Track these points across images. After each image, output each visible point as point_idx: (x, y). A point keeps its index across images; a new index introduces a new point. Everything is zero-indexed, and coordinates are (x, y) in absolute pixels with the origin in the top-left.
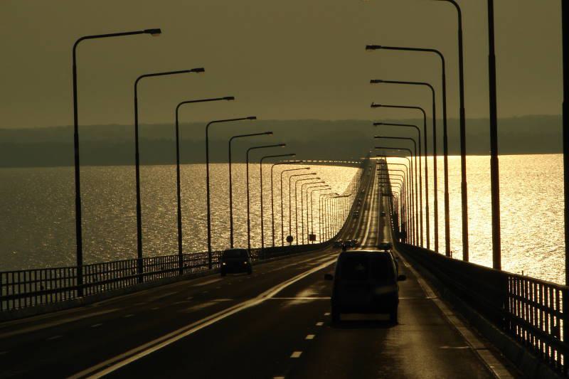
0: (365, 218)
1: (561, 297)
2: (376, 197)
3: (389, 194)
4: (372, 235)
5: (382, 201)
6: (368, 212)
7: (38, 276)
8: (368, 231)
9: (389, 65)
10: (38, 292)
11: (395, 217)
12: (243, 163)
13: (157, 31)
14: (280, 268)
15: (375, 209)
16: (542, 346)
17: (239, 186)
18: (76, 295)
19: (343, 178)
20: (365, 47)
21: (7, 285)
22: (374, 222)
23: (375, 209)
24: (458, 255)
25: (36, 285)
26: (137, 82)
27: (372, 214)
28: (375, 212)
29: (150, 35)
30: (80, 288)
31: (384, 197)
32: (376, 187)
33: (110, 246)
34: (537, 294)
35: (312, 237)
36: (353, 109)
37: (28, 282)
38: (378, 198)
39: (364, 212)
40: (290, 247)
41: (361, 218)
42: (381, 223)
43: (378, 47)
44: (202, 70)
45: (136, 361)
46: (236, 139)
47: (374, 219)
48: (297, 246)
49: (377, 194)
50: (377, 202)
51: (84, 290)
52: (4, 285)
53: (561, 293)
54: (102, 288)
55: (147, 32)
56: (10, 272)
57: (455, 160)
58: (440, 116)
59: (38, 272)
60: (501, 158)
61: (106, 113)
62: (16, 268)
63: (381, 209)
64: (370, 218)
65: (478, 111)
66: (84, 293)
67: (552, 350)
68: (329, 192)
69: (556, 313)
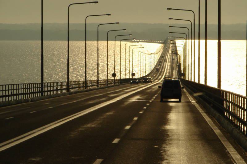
0: (164, 66)
1: (245, 102)
2: (170, 56)
3: (176, 53)
4: (167, 74)
6: (166, 63)
7: (33, 86)
10: (10, 95)
11: (179, 66)
12: (119, 41)
14: (245, 132)
15: (169, 62)
16: (237, 123)
18: (40, 95)
19: (156, 48)
21: (3, 91)
22: (169, 68)
23: (169, 62)
25: (21, 90)
28: (169, 63)
30: (86, 87)
33: (55, 75)
34: (235, 101)
35: (133, 74)
36: (162, 19)
38: (171, 57)
40: (133, 79)
41: (162, 66)
42: (172, 68)
43: (172, 27)
44: (97, 2)
45: (78, 117)
47: (169, 66)
48: (120, 80)
50: (171, 59)
51: (44, 93)
52: (1, 91)
53: (245, 100)
54: (52, 93)
55: (107, 15)
59: (15, 85)
61: (55, 18)
64: (167, 66)
65: (213, 21)
66: (44, 95)
67: (243, 126)
68: (143, 49)
69: (243, 109)
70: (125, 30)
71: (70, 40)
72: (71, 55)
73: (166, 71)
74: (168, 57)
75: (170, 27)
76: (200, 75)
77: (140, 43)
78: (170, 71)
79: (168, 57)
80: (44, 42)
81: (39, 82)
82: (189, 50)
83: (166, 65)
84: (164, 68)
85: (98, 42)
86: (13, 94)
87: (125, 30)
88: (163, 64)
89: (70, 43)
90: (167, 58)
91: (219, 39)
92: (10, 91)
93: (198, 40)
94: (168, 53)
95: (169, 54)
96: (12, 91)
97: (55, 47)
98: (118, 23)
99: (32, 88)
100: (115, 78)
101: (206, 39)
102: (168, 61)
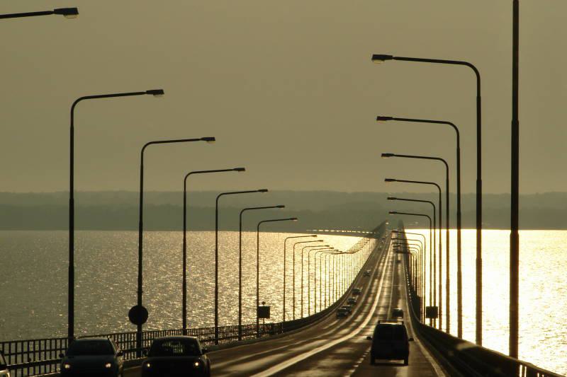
0: (374, 288)
2: (390, 264)
4: (381, 311)
5: (396, 270)
6: (379, 281)
7: (37, 346)
8: (375, 305)
9: (399, 138)
12: (252, 231)
13: (159, 92)
15: (387, 278)
17: (249, 252)
20: (381, 155)
22: (385, 294)
23: (387, 278)
24: (469, 336)
26: (145, 146)
27: (383, 284)
28: (387, 282)
29: (62, 16)
31: (399, 255)
32: (391, 254)
35: (263, 312)
36: (367, 180)
37: (37, 351)
38: (392, 266)
39: (373, 281)
41: (368, 288)
42: (395, 295)
46: (290, 239)
47: (386, 290)
49: (392, 262)
50: (391, 270)
55: (149, 92)
56: (20, 341)
57: (469, 234)
58: (453, 190)
60: (521, 232)
61: (106, 179)
62: (21, 337)
63: (395, 279)
64: (380, 289)
65: (497, 186)
70: (283, 207)
71: (145, 230)
72: (223, 264)
73: (379, 303)
74: (385, 268)
75: (389, 198)
76: (484, 309)
77: (320, 237)
78: (389, 303)
79: (385, 268)
80: (76, 232)
81: (61, 336)
82: (435, 255)
83: (377, 287)
84: (372, 295)
85: (217, 234)
86: (32, 361)
87: (283, 207)
88: (370, 284)
89: (187, 237)
90: (382, 268)
91: (515, 228)
92: (19, 357)
93: (474, 231)
94: (386, 257)
95: (387, 260)
96: (31, 356)
97: (106, 248)
98: (266, 191)
99: (28, 352)
100: (140, 328)
101: (459, 227)
102: (385, 276)
